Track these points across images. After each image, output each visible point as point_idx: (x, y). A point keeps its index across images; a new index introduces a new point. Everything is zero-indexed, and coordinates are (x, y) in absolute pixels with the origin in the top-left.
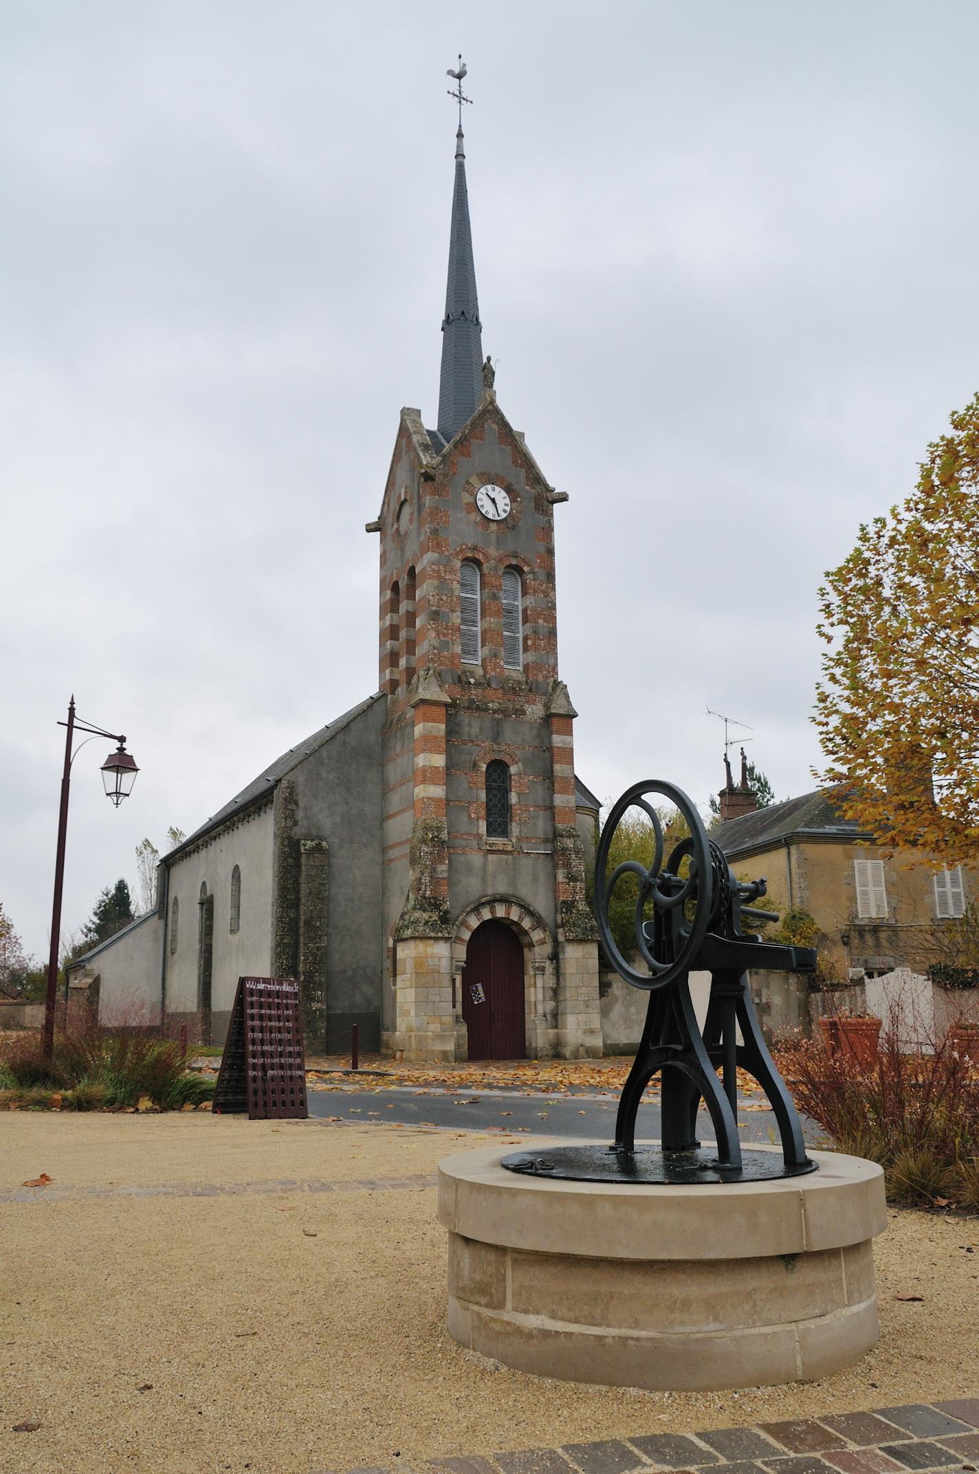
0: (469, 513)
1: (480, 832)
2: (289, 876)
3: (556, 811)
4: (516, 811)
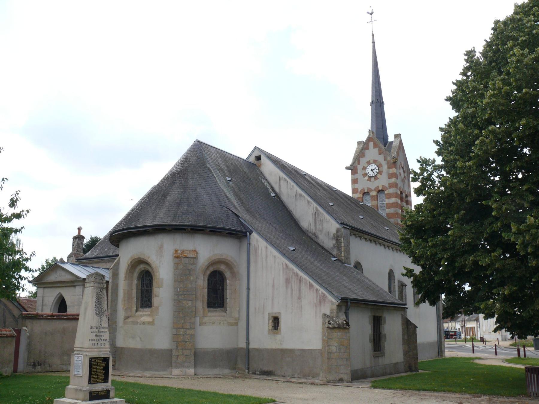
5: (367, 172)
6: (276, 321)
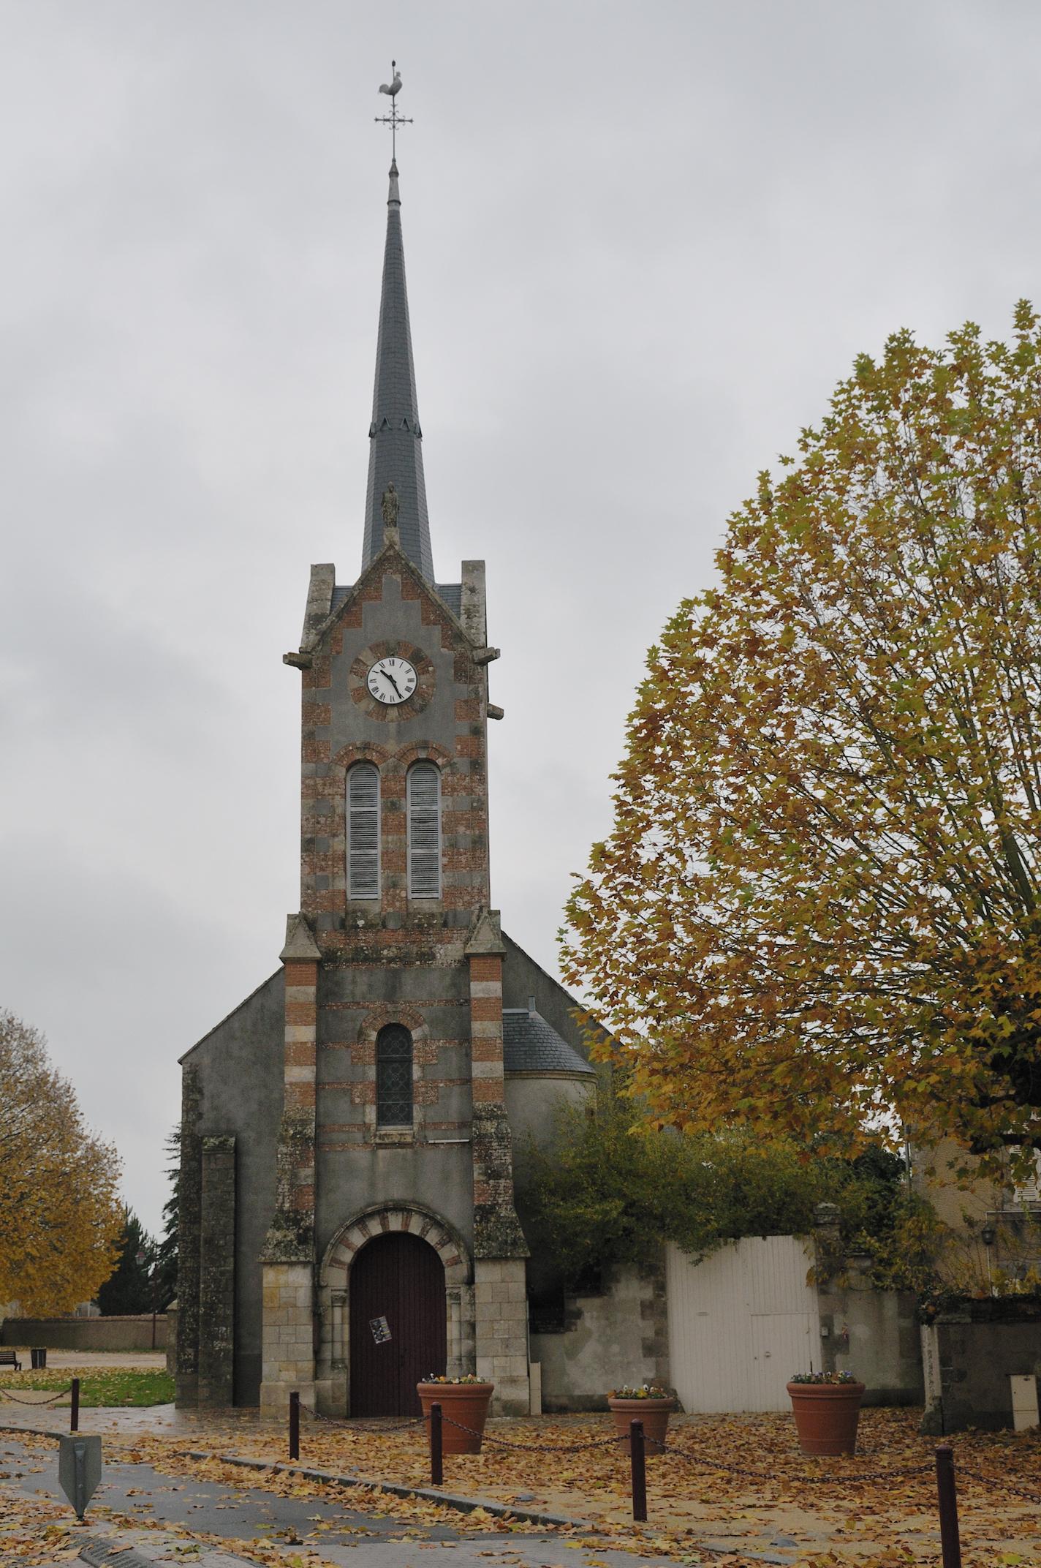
0: (358, 700)
1: (367, 1121)
2: (192, 1182)
3: (475, 1084)
4: (419, 1088)
5: (371, 686)
6: (704, 1314)
